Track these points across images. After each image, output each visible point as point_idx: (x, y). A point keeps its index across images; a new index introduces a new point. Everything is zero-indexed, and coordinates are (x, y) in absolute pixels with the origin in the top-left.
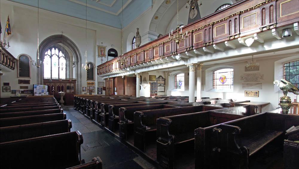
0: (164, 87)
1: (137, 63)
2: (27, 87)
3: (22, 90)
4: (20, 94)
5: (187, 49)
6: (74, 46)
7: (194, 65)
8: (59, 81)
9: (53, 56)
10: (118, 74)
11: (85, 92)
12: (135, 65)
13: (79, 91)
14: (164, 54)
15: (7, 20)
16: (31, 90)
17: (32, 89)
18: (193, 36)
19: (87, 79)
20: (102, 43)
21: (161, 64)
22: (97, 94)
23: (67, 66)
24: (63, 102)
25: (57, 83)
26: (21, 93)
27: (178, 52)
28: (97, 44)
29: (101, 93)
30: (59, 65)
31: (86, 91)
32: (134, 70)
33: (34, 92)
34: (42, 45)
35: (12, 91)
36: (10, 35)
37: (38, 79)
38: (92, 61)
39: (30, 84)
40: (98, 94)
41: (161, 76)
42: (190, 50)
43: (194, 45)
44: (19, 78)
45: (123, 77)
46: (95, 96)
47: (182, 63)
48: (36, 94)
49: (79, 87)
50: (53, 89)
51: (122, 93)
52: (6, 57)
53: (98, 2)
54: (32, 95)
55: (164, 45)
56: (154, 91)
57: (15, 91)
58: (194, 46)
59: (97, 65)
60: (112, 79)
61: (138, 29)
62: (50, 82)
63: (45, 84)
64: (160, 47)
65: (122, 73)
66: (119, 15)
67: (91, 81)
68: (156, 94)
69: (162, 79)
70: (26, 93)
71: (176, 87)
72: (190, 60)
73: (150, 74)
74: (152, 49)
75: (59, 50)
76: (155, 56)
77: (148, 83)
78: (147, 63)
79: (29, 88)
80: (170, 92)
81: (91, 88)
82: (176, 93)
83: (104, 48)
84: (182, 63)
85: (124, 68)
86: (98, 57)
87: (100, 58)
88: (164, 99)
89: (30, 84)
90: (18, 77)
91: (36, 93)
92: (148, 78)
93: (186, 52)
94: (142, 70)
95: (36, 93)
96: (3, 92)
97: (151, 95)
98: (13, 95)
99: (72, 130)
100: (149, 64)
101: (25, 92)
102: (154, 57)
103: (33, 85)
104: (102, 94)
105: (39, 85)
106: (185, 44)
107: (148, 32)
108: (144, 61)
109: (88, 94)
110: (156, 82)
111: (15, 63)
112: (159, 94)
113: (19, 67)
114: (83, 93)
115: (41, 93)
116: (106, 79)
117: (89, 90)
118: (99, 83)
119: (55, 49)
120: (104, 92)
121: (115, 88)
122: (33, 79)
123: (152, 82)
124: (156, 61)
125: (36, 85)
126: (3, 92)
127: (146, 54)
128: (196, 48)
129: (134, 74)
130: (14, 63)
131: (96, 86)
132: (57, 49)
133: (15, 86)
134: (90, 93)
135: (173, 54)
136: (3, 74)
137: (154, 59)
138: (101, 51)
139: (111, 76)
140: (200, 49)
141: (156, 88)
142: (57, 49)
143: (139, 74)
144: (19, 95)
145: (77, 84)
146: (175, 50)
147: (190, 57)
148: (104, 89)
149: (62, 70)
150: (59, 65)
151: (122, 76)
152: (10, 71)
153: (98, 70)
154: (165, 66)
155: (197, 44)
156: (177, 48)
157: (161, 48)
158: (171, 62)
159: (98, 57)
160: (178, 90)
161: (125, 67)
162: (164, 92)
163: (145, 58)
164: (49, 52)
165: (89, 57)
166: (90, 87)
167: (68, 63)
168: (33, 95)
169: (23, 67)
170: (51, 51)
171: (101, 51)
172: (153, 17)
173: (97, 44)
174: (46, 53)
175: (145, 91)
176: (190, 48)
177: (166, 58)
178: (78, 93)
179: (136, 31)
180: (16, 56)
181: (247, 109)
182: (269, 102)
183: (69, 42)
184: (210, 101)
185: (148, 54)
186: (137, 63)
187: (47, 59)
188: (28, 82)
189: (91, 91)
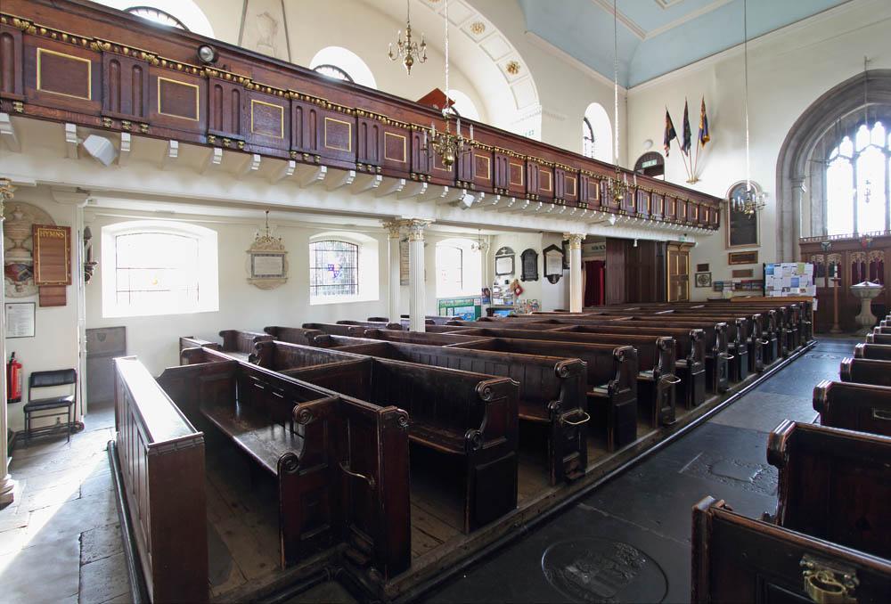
2: (749, 273)
3: (738, 280)
9: (861, 154)
17: (762, 278)
26: (734, 288)
30: (855, 186)
33: (767, 285)
34: (792, 138)
35: (715, 283)
36: (707, 144)
37: (782, 247)
39: (757, 262)
48: (771, 293)
50: (836, 275)
57: (722, 283)
62: (826, 253)
63: (805, 260)
70: (746, 290)
79: (757, 276)
89: (757, 262)
90: (727, 248)
91: (772, 289)
95: (772, 289)
96: (696, 286)
98: (716, 295)
99: (812, 417)
101: (745, 287)
103: (764, 265)
105: (785, 264)
113: (731, 220)
115: (788, 289)
122: (767, 245)
125: (771, 265)
126: (696, 286)
130: (718, 211)
133: (722, 271)
136: (694, 244)
144: (728, 293)
149: (867, 201)
150: (855, 186)
164: (846, 146)
168: (764, 295)
181: (225, 340)
182: (104, 456)
184: (852, 263)
188: (752, 258)
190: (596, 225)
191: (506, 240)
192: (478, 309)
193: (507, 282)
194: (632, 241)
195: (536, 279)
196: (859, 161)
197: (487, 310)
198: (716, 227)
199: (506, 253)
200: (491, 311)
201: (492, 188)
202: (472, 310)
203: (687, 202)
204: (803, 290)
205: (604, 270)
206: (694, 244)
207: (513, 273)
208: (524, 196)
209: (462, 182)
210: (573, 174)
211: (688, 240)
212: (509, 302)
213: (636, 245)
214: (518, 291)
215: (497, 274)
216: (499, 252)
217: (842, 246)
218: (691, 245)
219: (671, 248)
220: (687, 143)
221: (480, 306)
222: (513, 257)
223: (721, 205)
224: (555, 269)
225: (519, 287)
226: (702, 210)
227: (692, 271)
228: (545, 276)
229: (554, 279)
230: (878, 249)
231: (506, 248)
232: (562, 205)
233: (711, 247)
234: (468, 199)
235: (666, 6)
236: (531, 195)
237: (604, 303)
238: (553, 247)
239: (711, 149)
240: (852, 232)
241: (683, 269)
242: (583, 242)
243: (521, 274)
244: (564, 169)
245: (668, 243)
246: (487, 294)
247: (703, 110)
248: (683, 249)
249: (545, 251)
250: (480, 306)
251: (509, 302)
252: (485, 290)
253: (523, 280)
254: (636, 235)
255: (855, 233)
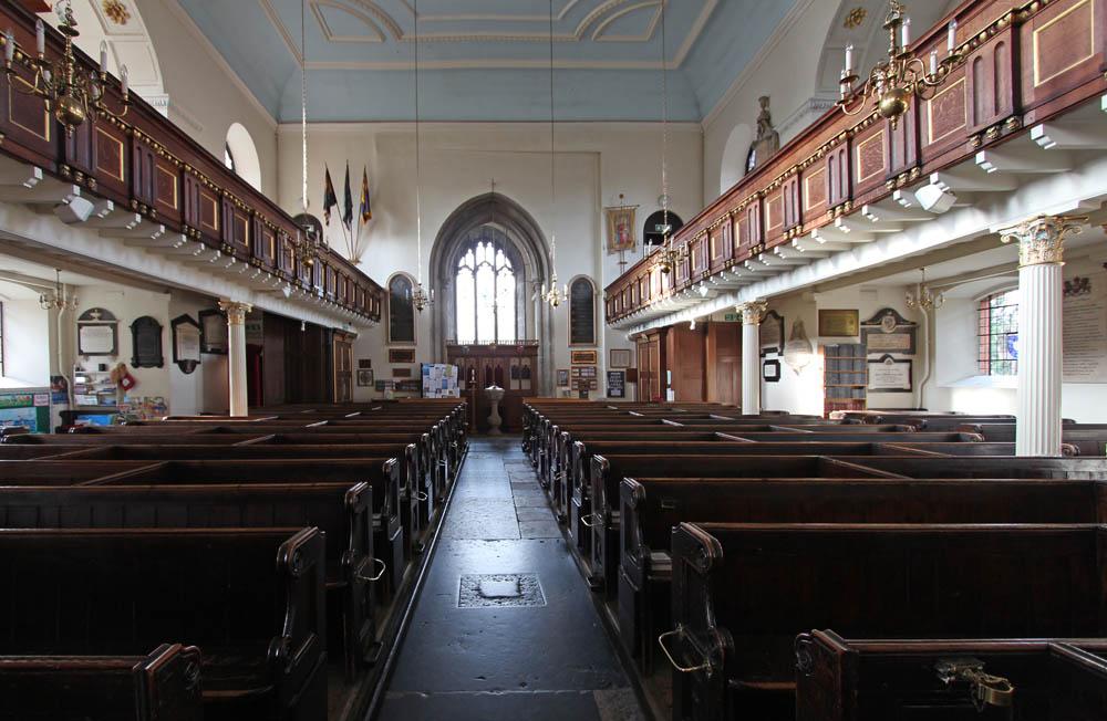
0: (906, 365)
1: (735, 259)
2: (407, 372)
3: (398, 380)
4: (391, 392)
5: (983, 132)
6: (530, 226)
7: (1056, 225)
8: (499, 350)
10: (675, 312)
11: (564, 389)
12: (728, 269)
13: (547, 385)
14: (855, 193)
15: (362, 178)
16: (416, 382)
18: (1024, 42)
19: (573, 342)
20: (621, 196)
21: (853, 247)
22: (605, 395)
23: (520, 297)
24: (500, 420)
25: (483, 356)
27: (926, 169)
28: (605, 204)
29: (619, 393)
30: (495, 296)
31: (566, 385)
32: (734, 292)
35: (377, 382)
36: (369, 221)
38: (588, 272)
40: (609, 395)
41: (890, 310)
42: (1006, 136)
43: (1028, 99)
44: (391, 344)
45: (692, 327)
46: (602, 405)
47: (970, 224)
48: (427, 394)
49: (548, 372)
51: (696, 397)
52: (356, 285)
53: (602, 38)
54: (418, 394)
55: (855, 141)
56: (845, 384)
57: (383, 382)
58: (1029, 109)
59: (604, 284)
60: (657, 337)
61: (765, 101)
64: (831, 158)
65: (688, 307)
66: (685, 63)
67: (584, 349)
68: (861, 403)
69: (903, 318)
71: (986, 363)
72: (1021, 202)
73: (824, 301)
74: (795, 178)
75: (497, 247)
76: (808, 213)
77: (815, 350)
78: (776, 250)
79: (414, 375)
80: (947, 391)
81: (586, 374)
82: (974, 398)
83: (630, 215)
84: (970, 224)
85: (689, 287)
86: (610, 253)
87: (616, 258)
88: (882, 430)
90: (388, 343)
92: (812, 324)
93: (980, 157)
94: (763, 285)
96: (359, 385)
97: (829, 407)
100: (784, 254)
102: (807, 218)
104: (623, 395)
106: (967, 114)
107: (812, 100)
108: (762, 242)
109: (576, 395)
110: (858, 340)
111: (383, 302)
112: (876, 403)
114: (559, 392)
116: (636, 338)
117: (579, 381)
118: (612, 352)
119: (485, 245)
120: (631, 387)
121: (669, 372)
123: (833, 342)
124: (814, 233)
127: (772, 208)
128: (1046, 111)
129: (734, 309)
130: (379, 301)
131: (603, 366)
132: (490, 244)
133: (383, 370)
134: (581, 392)
135: (902, 180)
136: (356, 335)
137: (806, 228)
138: (620, 228)
139: (652, 326)
140: (1087, 110)
141: (858, 368)
142: (490, 244)
143: (751, 307)
144: (390, 394)
145: (539, 358)
146: (912, 158)
147: (1023, 182)
148: (632, 375)
150: (495, 296)
151: (690, 323)
152: (371, 327)
153: (607, 302)
154: (872, 256)
155: (1055, 90)
156: (854, 184)
157: (839, 163)
158: (906, 227)
159: (610, 253)
160: (997, 379)
161: (693, 281)
162: (910, 391)
163: (768, 228)
164: (468, 259)
165: (579, 255)
166: (580, 368)
167: (520, 285)
169: (396, 308)
170: (474, 252)
171: (620, 228)
172: (836, 21)
173: (605, 204)
174: (461, 264)
175: (801, 386)
176: (1002, 123)
177: (865, 210)
178: (544, 390)
179: (757, 112)
180: (383, 283)
183: (514, 214)
185: (780, 209)
186: (733, 257)
187: (463, 280)
188: (408, 356)
189: (585, 386)
190: (262, 295)
191: (99, 295)
192: (43, 413)
193: (103, 368)
194: (298, 322)
195: (160, 364)
196: (478, 273)
197: (62, 414)
198: (378, 319)
199: (100, 318)
200: (69, 417)
201: (126, 200)
202: (30, 414)
203: (356, 285)
204: (450, 392)
205: (261, 358)
206: (356, 335)
207: (115, 353)
208: (178, 227)
209: (73, 170)
210: (244, 213)
211: (351, 330)
212: (109, 400)
213: (303, 329)
214: (126, 382)
215: (81, 353)
216: (86, 316)
217: (477, 350)
218: (353, 336)
219: (337, 338)
220: (348, 216)
221: (47, 407)
222: (114, 327)
223: (382, 295)
224: (190, 353)
225: (128, 376)
226: (359, 291)
227: (355, 367)
228: (175, 360)
229: (189, 367)
230: (502, 356)
231: (100, 310)
232: (231, 255)
233: (371, 340)
234: (82, 207)
235: (331, 39)
236: (190, 228)
237: (262, 404)
238: (185, 318)
239: (371, 230)
240: (514, 338)
241: (347, 363)
242: (247, 315)
243: (131, 355)
244: (234, 203)
245: (335, 330)
246: (61, 386)
247: (365, 181)
248: (347, 341)
249: (174, 323)
250: (47, 407)
251: (109, 400)
252: (55, 380)
253: (136, 364)
254: (305, 316)
255: (476, 341)
